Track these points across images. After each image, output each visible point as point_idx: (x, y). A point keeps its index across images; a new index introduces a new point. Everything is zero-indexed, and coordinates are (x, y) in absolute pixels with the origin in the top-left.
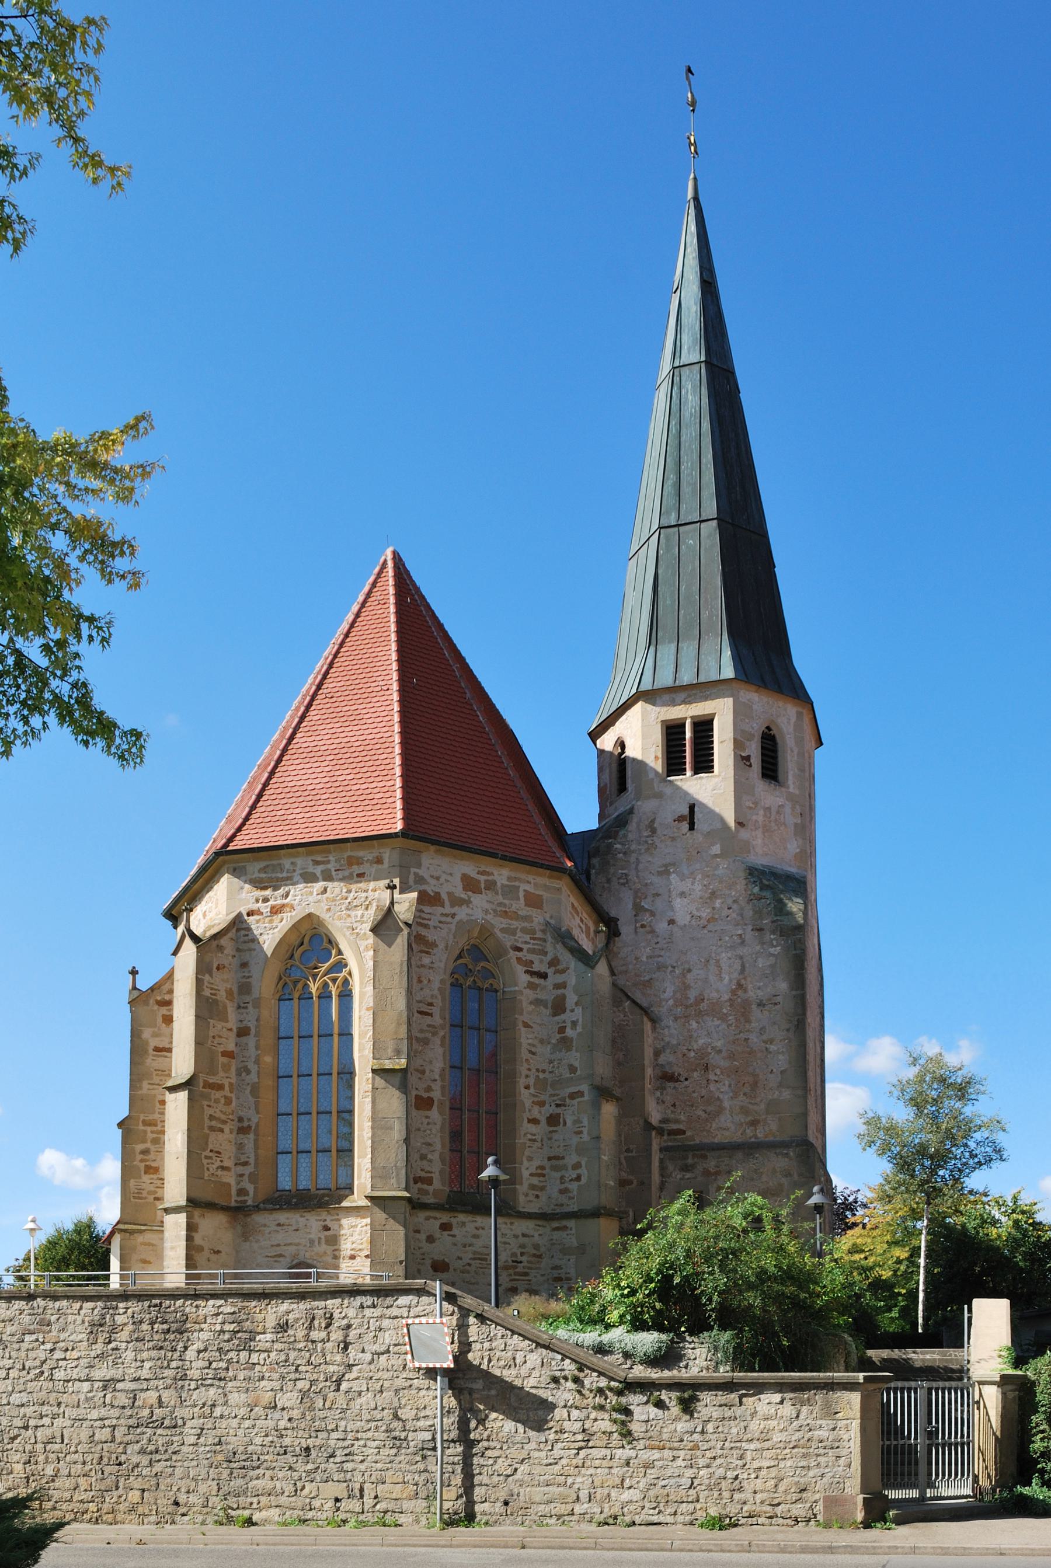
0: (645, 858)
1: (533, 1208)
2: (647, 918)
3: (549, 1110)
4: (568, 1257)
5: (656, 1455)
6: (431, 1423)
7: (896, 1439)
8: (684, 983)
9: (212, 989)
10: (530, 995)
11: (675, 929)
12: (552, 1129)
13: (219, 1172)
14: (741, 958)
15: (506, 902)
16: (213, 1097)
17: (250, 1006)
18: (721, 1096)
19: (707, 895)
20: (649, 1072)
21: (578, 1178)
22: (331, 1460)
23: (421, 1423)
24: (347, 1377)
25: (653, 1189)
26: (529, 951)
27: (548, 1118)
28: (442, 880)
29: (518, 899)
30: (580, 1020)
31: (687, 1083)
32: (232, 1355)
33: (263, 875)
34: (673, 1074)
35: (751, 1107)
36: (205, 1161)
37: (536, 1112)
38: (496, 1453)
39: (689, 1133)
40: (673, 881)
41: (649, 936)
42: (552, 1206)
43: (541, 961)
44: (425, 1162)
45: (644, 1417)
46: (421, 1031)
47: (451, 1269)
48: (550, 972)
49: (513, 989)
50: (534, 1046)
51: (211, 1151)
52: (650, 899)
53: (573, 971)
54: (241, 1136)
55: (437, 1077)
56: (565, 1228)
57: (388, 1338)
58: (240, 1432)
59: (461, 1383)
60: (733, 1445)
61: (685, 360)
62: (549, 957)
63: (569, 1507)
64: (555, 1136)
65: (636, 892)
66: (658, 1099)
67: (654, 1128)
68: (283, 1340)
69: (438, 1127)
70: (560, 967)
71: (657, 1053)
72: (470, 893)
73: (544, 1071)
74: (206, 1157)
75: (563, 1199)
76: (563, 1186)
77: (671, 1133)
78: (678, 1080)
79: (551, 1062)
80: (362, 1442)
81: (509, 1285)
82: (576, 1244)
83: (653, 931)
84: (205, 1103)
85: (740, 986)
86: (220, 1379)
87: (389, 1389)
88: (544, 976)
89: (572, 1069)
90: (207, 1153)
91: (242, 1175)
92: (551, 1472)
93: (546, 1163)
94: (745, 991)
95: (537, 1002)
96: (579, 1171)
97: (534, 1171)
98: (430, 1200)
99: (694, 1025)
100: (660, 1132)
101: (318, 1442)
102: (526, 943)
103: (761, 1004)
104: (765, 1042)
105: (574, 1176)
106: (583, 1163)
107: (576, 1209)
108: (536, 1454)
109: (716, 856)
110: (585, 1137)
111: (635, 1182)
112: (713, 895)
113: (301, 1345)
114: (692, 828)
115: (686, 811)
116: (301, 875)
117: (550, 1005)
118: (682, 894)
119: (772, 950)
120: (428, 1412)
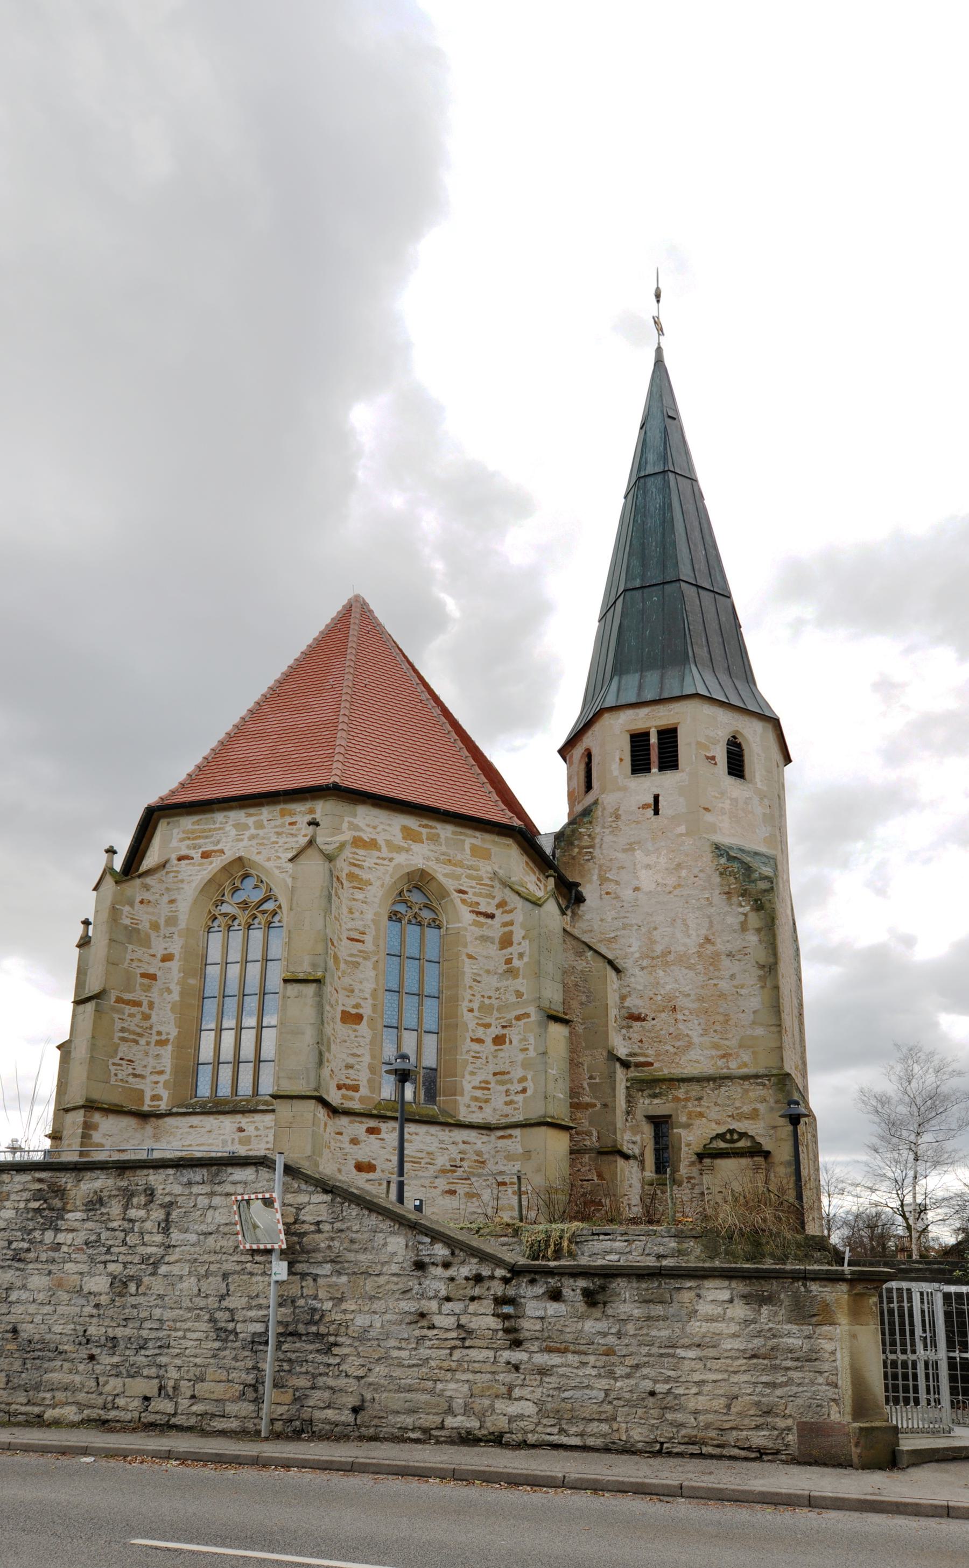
0: (608, 838)
1: (477, 1118)
2: (611, 887)
3: (495, 1031)
4: (513, 1163)
5: (555, 1359)
6: (265, 1312)
7: (904, 1352)
8: (650, 939)
9: (132, 919)
10: (478, 931)
11: (640, 895)
12: (497, 1048)
13: (131, 1079)
14: (709, 917)
15: (451, 852)
16: (127, 1012)
17: (175, 936)
18: (690, 1032)
19: (673, 866)
20: (613, 1012)
21: (524, 1091)
22: (143, 1352)
23: (252, 1314)
24: (167, 1259)
25: (618, 1111)
26: (475, 894)
27: (493, 1039)
28: (379, 829)
29: (464, 850)
30: (527, 953)
31: (654, 1022)
32: (37, 1234)
33: (197, 827)
34: (640, 1014)
35: (722, 1042)
36: (112, 1068)
37: (480, 1033)
38: (345, 1350)
39: (656, 1065)
40: (638, 857)
41: (614, 902)
42: (497, 1117)
43: (489, 903)
44: (351, 1071)
45: (540, 1313)
46: (351, 955)
47: (378, 1170)
48: (498, 913)
49: (456, 925)
50: (479, 975)
51: (121, 1059)
52: (613, 872)
53: (520, 911)
54: (158, 1047)
55: (368, 996)
56: (511, 1136)
57: (219, 1217)
58: (38, 1319)
59: (300, 1267)
60: (663, 1351)
61: (650, 470)
62: (497, 901)
63: (438, 1419)
64: (501, 1054)
65: (600, 866)
66: (624, 1035)
67: (619, 1059)
68: (95, 1218)
69: (368, 1040)
70: (507, 908)
71: (623, 998)
72: (410, 842)
73: (490, 997)
74: (114, 1064)
75: (508, 1110)
76: (508, 1099)
77: (638, 1065)
78: (644, 1020)
79: (497, 989)
80: (180, 1334)
81: (447, 1188)
82: (521, 1151)
83: (617, 897)
84: (116, 1016)
85: (708, 940)
86: (20, 1260)
87: (214, 1274)
88: (492, 916)
89: (519, 994)
90: (117, 1061)
91: (157, 1083)
92: (416, 1375)
93: (490, 1078)
94: (713, 944)
95: (484, 939)
96: (524, 1084)
97: (477, 1084)
98: (356, 1105)
99: (661, 973)
100: (626, 1065)
101: (128, 1332)
102: (471, 887)
103: (730, 955)
104: (735, 987)
105: (520, 1089)
106: (529, 1077)
107: (521, 1119)
108: (395, 1353)
109: (681, 835)
110: (532, 1053)
111: (599, 1106)
112: (679, 866)
113: (115, 1225)
114: (656, 812)
115: (651, 800)
116: (233, 825)
117: (497, 941)
118: (648, 867)
119: (741, 910)
120: (262, 1301)
